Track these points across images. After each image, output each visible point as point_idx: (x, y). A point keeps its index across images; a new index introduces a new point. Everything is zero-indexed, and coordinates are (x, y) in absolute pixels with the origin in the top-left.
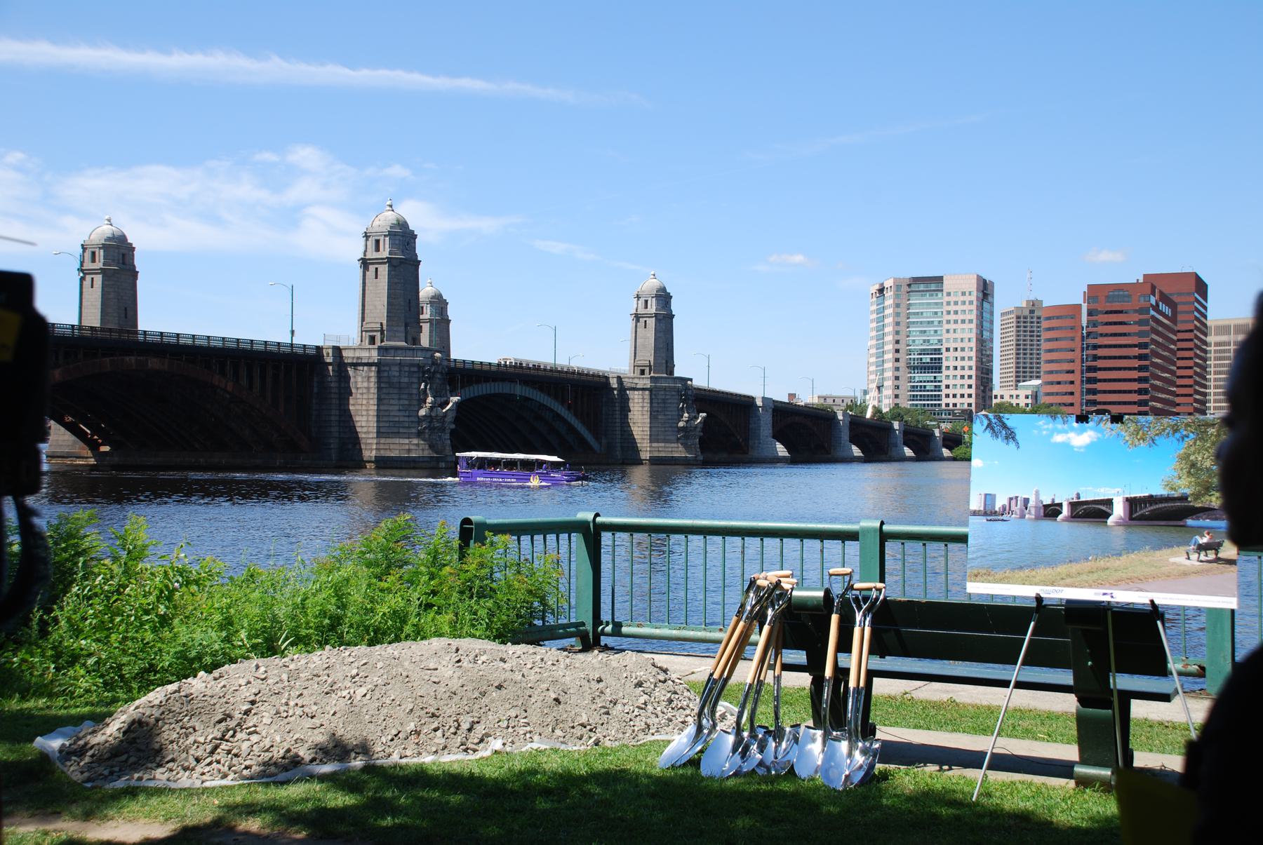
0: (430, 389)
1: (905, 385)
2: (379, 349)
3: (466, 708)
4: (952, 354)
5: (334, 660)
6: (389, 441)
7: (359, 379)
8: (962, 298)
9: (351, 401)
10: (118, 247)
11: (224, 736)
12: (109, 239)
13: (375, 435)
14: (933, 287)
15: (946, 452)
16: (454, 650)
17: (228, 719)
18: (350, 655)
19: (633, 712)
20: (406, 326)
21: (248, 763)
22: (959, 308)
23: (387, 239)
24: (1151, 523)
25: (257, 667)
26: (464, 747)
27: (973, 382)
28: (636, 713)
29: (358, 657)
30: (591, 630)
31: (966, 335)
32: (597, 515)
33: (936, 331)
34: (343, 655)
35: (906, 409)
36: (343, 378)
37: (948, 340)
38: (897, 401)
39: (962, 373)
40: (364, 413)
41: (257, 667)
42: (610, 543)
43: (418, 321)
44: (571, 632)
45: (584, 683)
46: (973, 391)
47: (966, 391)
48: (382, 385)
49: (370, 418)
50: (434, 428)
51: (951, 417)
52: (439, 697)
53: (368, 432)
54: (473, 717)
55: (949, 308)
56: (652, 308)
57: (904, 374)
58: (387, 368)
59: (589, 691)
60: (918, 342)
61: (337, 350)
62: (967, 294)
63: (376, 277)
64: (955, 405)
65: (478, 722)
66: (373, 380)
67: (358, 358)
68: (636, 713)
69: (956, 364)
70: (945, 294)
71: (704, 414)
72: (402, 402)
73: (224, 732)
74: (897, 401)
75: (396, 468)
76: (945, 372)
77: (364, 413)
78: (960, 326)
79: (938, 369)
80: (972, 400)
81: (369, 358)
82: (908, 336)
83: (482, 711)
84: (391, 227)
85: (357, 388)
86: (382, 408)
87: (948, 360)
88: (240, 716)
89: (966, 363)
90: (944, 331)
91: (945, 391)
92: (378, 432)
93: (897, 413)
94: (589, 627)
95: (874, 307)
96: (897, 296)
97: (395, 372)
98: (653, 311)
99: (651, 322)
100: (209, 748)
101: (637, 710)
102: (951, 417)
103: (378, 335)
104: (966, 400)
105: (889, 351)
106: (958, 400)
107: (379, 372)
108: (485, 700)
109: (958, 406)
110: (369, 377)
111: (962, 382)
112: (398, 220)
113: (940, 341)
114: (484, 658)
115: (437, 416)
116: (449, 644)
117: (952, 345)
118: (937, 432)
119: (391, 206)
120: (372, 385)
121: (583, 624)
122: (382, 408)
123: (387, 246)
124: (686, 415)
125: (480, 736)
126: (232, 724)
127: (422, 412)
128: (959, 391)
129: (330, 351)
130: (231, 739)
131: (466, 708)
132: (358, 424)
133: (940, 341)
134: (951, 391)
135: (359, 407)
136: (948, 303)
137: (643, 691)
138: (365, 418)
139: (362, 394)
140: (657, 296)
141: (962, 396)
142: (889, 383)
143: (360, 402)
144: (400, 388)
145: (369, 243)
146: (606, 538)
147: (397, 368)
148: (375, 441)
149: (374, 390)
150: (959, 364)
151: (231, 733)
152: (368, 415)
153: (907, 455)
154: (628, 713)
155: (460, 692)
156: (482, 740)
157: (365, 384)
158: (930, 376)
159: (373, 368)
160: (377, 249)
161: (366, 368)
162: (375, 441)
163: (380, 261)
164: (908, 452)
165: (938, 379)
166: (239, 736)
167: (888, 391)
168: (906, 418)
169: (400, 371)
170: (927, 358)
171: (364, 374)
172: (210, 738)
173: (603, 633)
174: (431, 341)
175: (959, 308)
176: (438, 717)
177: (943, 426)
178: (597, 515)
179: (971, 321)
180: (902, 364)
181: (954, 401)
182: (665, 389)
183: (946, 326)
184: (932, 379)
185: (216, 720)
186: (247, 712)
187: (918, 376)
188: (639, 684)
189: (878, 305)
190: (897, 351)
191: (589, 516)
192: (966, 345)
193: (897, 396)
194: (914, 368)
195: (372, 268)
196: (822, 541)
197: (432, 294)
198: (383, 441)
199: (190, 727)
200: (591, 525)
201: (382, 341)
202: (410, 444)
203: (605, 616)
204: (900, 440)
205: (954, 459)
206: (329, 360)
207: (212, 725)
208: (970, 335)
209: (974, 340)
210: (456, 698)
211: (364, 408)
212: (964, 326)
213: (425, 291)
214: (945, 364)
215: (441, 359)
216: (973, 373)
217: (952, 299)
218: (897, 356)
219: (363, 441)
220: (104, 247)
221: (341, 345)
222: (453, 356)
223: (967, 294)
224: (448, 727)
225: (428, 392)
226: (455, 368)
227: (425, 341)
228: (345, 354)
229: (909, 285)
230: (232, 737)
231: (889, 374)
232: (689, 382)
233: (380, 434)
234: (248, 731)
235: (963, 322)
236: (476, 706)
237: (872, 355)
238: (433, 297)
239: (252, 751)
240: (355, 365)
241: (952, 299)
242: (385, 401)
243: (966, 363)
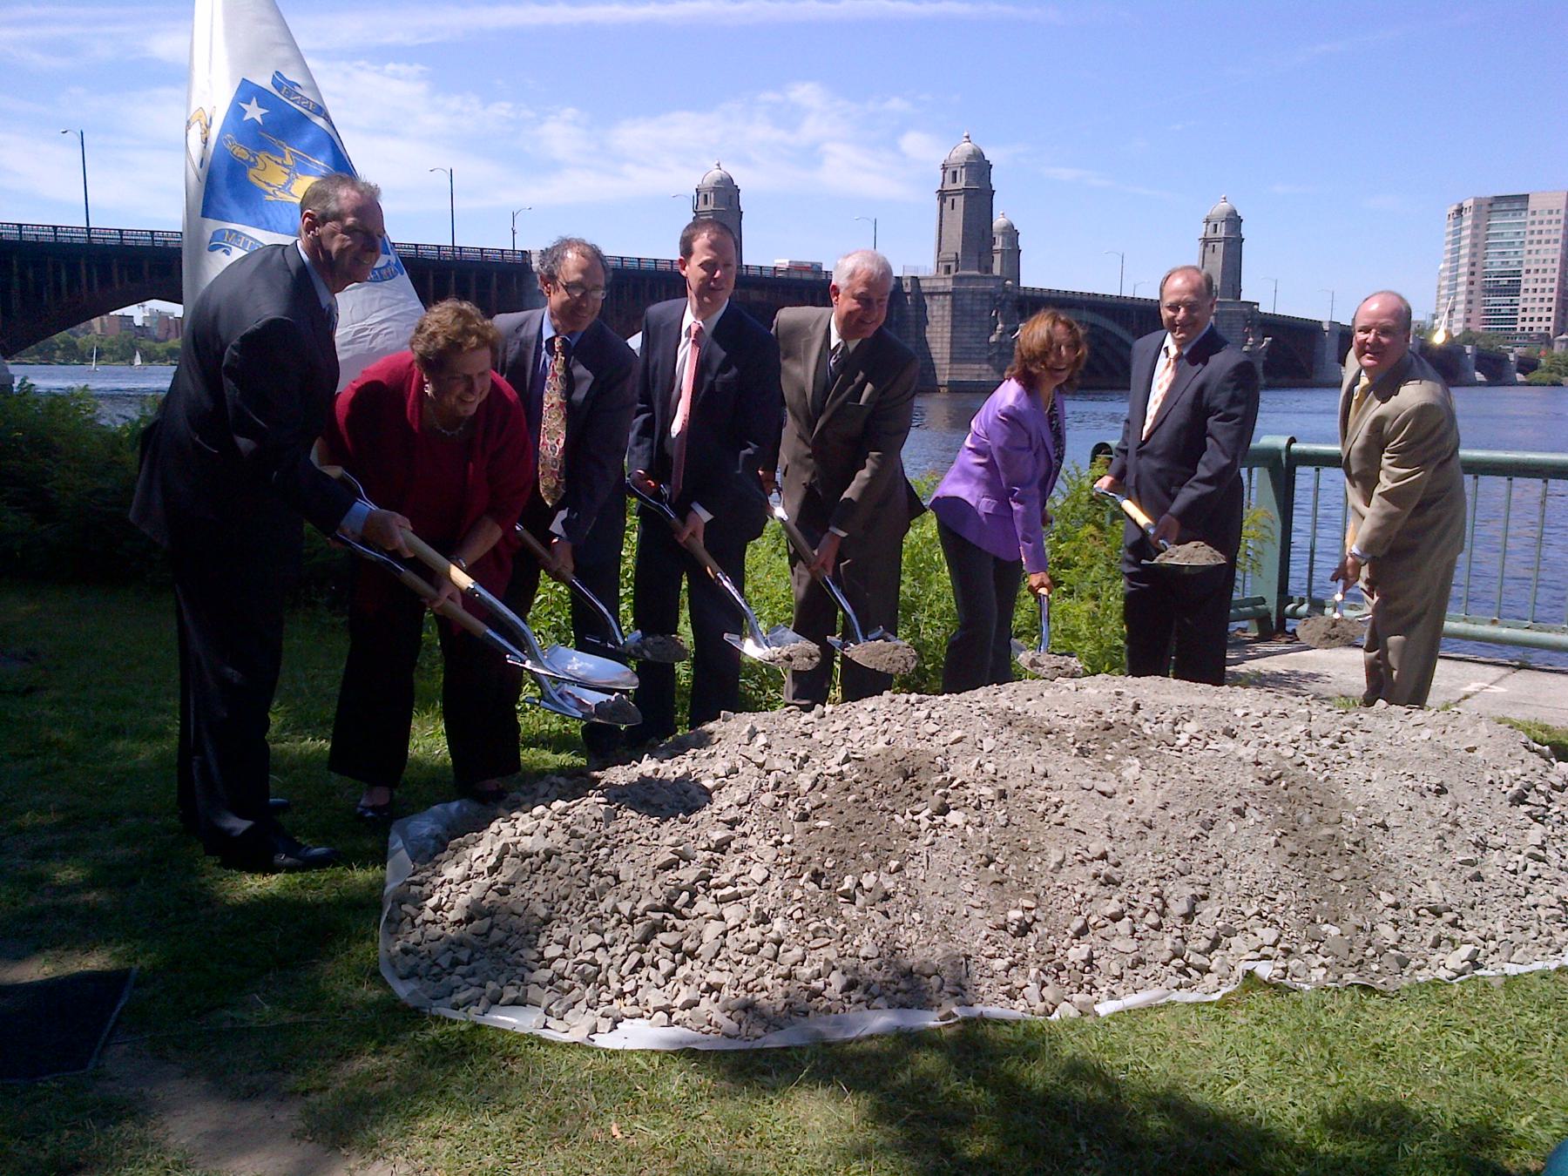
0: (1001, 316)
1: (1479, 310)
2: (955, 278)
3: (1178, 862)
4: (1532, 276)
5: (898, 728)
6: (961, 366)
7: (935, 308)
8: (1549, 217)
9: (928, 329)
10: (725, 190)
12: (718, 182)
13: (948, 361)
14: (1517, 206)
15: (1520, 377)
16: (1130, 708)
17: (682, 864)
18: (929, 717)
19: (1525, 868)
20: (979, 256)
21: (713, 977)
22: (1545, 227)
23: (964, 170)
25: (753, 734)
26: (1178, 962)
27: (1553, 305)
28: (1530, 872)
29: (943, 723)
30: (1275, 610)
31: (1550, 257)
32: (1292, 440)
33: (1516, 252)
34: (916, 714)
35: (1477, 333)
36: (922, 308)
37: (1529, 261)
38: (1469, 325)
39: (1542, 295)
40: (939, 340)
41: (753, 734)
42: (1311, 483)
43: (991, 251)
44: (1246, 612)
45: (1413, 799)
46: (1552, 314)
47: (1545, 314)
48: (956, 313)
49: (944, 345)
50: (1003, 354)
51: (1526, 341)
52: (1116, 834)
53: (942, 359)
54: (1192, 884)
55: (1533, 228)
56: (1222, 233)
57: (1478, 297)
58: (960, 297)
59: (1429, 821)
60: (1495, 264)
61: (915, 279)
62: (1555, 212)
63: (953, 208)
64: (1531, 329)
65: (1205, 898)
66: (948, 308)
67: (934, 288)
68: (1530, 872)
69: (1536, 286)
70: (1529, 213)
71: (1270, 339)
72: (973, 329)
73: (671, 893)
74: (1469, 325)
75: (967, 392)
76: (1523, 295)
77: (939, 329)
78: (1543, 246)
79: (1517, 293)
80: (1551, 324)
81: (944, 287)
82: (1485, 258)
83: (1212, 868)
84: (968, 159)
85: (933, 317)
86: (955, 334)
87: (1527, 282)
88: (707, 855)
89: (1547, 285)
90: (1525, 252)
91: (1521, 315)
92: (951, 358)
93: (1468, 336)
94: (1272, 605)
95: (1451, 229)
96: (1476, 216)
97: (968, 299)
98: (1222, 234)
99: (1220, 246)
101: (1532, 864)
102: (1526, 341)
103: (953, 265)
104: (1544, 324)
105: (1463, 274)
106: (1535, 324)
107: (953, 300)
108: (1214, 841)
109: (1535, 330)
110: (943, 307)
111: (1541, 305)
112: (974, 151)
113: (1520, 262)
114: (1191, 728)
115: (1006, 342)
116: (1118, 694)
117: (1533, 267)
118: (1512, 357)
119: (968, 137)
120: (946, 313)
121: (1263, 601)
122: (955, 334)
123: (963, 177)
124: (1251, 339)
125: (1211, 933)
126: (688, 874)
127: (993, 339)
128: (1536, 315)
129: (909, 282)
130: (685, 911)
131: (1178, 862)
132: (933, 351)
133: (1520, 262)
134: (1528, 315)
135: (934, 335)
136: (1533, 223)
137: (1529, 814)
138: (939, 345)
139: (937, 322)
140: (1227, 220)
141: (1540, 319)
142: (1461, 307)
143: (935, 329)
144: (973, 316)
145: (946, 175)
146: (1304, 477)
147: (970, 297)
148: (948, 367)
149: (948, 318)
150: (1539, 286)
151: (685, 895)
152: (942, 342)
153: (1478, 379)
154: (1514, 872)
155: (1162, 826)
156: (1215, 943)
157: (940, 313)
158: (1506, 299)
159: (948, 297)
160: (955, 181)
161: (941, 297)
162: (948, 367)
163: (957, 192)
164: (1479, 376)
165: (1516, 302)
166: (704, 905)
167: (1459, 315)
168: (1478, 342)
169: (972, 299)
170: (1504, 281)
171: (939, 303)
172: (642, 906)
173: (1294, 615)
174: (1002, 270)
175: (1545, 227)
176: (1119, 884)
177: (1517, 350)
178: (1292, 440)
179: (1556, 241)
180: (1475, 287)
181: (1531, 324)
182: (1230, 313)
183: (1529, 247)
184: (1509, 302)
185: (660, 862)
186: (722, 847)
187: (1494, 299)
188: (1519, 799)
189: (1455, 226)
190: (1473, 274)
191: (1282, 442)
192: (1549, 266)
193: (1468, 320)
194: (1490, 291)
195: (949, 199)
196: (1546, 482)
197: (1004, 225)
198: (955, 366)
199: (609, 874)
200: (1284, 455)
201: (956, 271)
202: (980, 369)
203: (1296, 585)
204: (1472, 367)
205: (1529, 384)
206: (908, 290)
207: (649, 873)
208: (1553, 256)
209: (1558, 261)
210: (1154, 838)
211: (939, 335)
212: (1548, 246)
213: (999, 221)
214: (1524, 286)
215: (1012, 286)
216: (1554, 295)
217: (1537, 218)
218: (1472, 278)
219: (937, 367)
220: (715, 190)
221: (919, 275)
222: (1022, 284)
223: (1555, 212)
224: (1141, 912)
225: (999, 319)
226: (1026, 297)
227: (997, 271)
228: (922, 284)
229: (1491, 205)
230: (686, 906)
231: (1462, 298)
232: (1256, 307)
233: (953, 360)
234: (720, 893)
235: (1548, 242)
236: (1198, 858)
237: (1444, 279)
238: (1005, 228)
239: (723, 946)
240: (931, 294)
241: (1537, 218)
242: (959, 329)
243: (1547, 285)
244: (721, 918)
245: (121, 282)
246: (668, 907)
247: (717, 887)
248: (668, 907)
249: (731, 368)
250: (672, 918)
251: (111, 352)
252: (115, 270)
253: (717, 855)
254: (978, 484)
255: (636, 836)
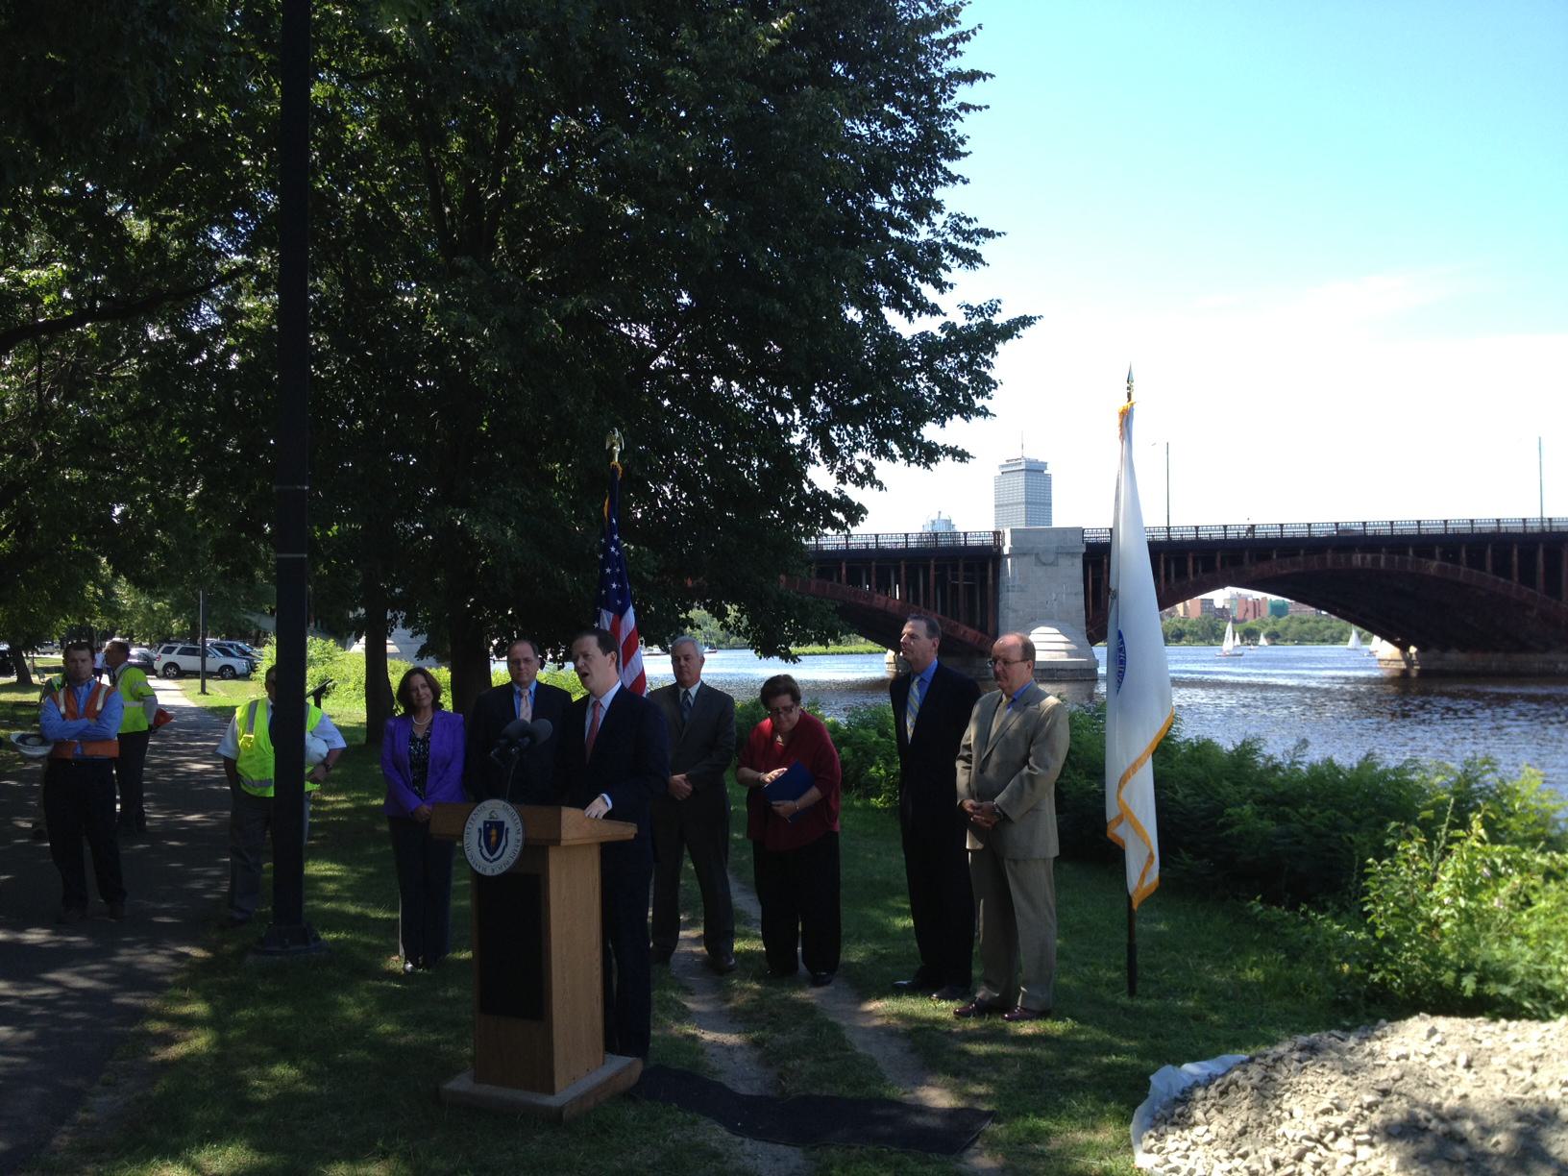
11: (1322, 1137)
24: (990, 592)
100: (1295, 1150)
244: (1354, 1154)
245: (1195, 572)
246: (1319, 1141)
247: (1358, 1134)
248: (1319, 1141)
249: (12, 674)
250: (1320, 1148)
251: (1192, 633)
252: (1190, 564)
253: (1366, 1113)
254: (1493, 1125)
255: (1310, 1088)
